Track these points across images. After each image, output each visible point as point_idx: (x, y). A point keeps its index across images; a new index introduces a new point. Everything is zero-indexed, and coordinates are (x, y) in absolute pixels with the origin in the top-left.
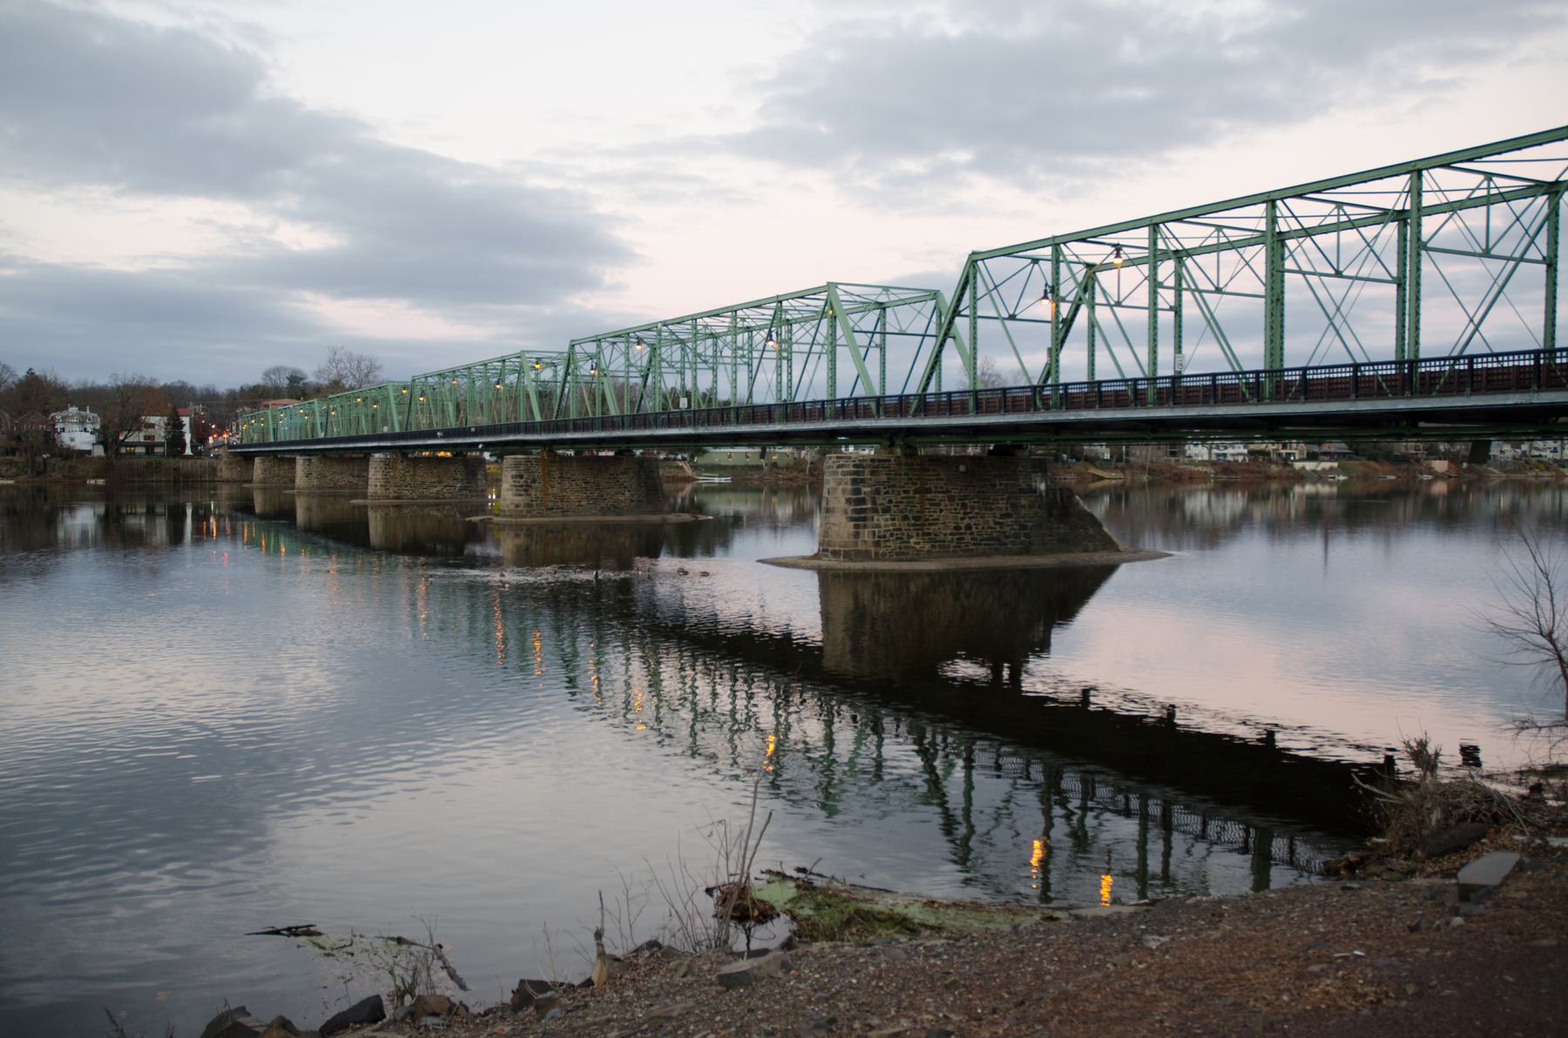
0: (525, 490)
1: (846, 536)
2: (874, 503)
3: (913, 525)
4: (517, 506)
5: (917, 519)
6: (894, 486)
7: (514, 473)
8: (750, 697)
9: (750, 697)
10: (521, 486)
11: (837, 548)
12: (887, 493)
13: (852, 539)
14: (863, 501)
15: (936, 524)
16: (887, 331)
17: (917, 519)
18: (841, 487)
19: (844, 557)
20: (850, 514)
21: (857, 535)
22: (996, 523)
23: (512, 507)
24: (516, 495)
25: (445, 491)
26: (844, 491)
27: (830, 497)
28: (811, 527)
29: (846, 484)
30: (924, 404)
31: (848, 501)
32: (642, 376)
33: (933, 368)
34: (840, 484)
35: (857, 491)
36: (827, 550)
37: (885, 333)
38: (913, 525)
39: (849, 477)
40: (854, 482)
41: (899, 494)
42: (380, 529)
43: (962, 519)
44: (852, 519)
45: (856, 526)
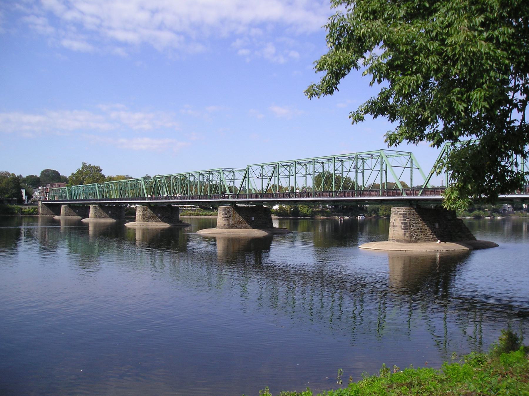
0: (228, 219)
1: (401, 234)
2: (410, 224)
3: (420, 231)
4: (225, 225)
5: (421, 229)
6: (415, 218)
7: (223, 213)
8: (341, 298)
9: (341, 298)
10: (226, 218)
11: (398, 239)
12: (413, 220)
13: (403, 236)
14: (406, 223)
15: (426, 231)
16: (413, 167)
17: (421, 229)
18: (399, 218)
19: (401, 242)
20: (402, 228)
21: (405, 235)
22: (442, 231)
23: (223, 225)
24: (224, 221)
25: (165, 219)
26: (400, 220)
27: (395, 222)
28: (503, 231)
29: (401, 217)
30: (425, 191)
31: (402, 223)
32: (269, 178)
33: (295, 182)
34: (399, 217)
35: (405, 220)
36: (394, 240)
37: (412, 168)
38: (420, 231)
39: (402, 215)
40: (404, 217)
41: (416, 221)
42: (141, 237)
43: (433, 229)
44: (403, 229)
45: (405, 232)
